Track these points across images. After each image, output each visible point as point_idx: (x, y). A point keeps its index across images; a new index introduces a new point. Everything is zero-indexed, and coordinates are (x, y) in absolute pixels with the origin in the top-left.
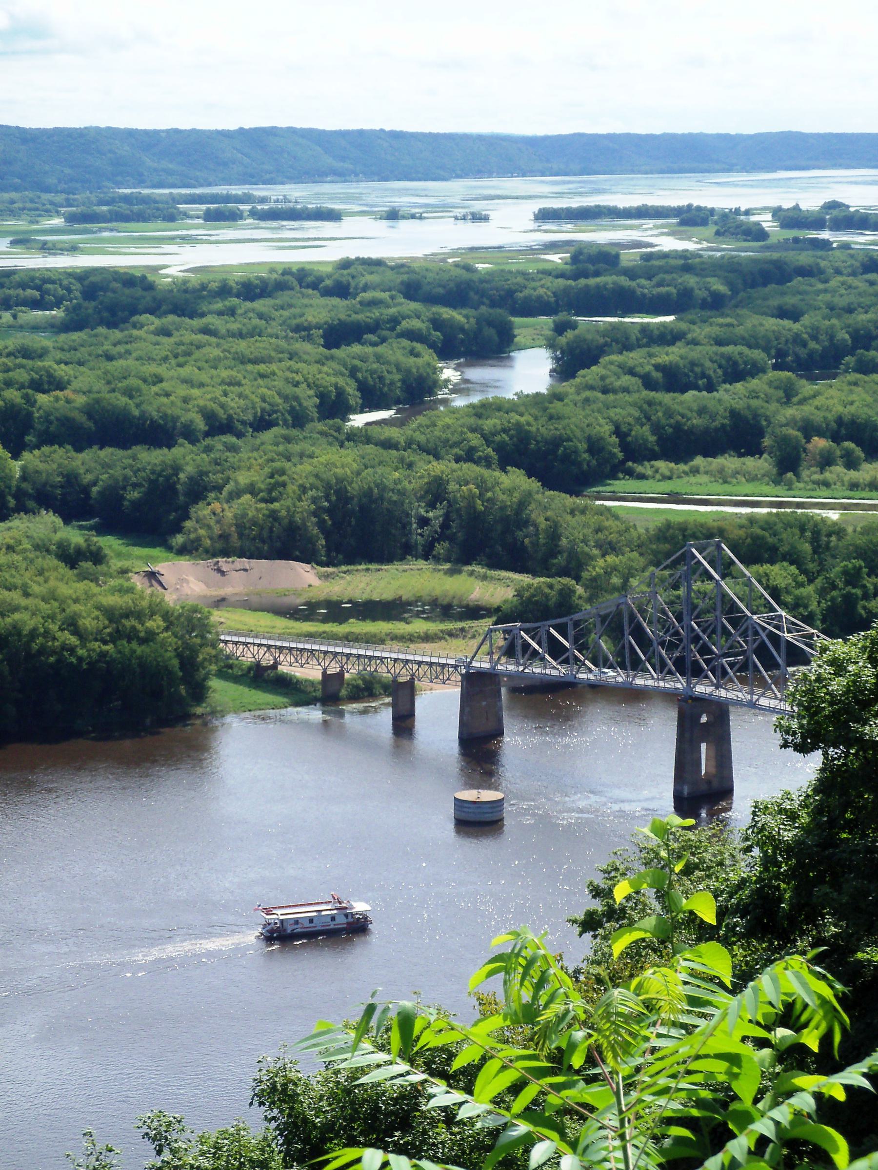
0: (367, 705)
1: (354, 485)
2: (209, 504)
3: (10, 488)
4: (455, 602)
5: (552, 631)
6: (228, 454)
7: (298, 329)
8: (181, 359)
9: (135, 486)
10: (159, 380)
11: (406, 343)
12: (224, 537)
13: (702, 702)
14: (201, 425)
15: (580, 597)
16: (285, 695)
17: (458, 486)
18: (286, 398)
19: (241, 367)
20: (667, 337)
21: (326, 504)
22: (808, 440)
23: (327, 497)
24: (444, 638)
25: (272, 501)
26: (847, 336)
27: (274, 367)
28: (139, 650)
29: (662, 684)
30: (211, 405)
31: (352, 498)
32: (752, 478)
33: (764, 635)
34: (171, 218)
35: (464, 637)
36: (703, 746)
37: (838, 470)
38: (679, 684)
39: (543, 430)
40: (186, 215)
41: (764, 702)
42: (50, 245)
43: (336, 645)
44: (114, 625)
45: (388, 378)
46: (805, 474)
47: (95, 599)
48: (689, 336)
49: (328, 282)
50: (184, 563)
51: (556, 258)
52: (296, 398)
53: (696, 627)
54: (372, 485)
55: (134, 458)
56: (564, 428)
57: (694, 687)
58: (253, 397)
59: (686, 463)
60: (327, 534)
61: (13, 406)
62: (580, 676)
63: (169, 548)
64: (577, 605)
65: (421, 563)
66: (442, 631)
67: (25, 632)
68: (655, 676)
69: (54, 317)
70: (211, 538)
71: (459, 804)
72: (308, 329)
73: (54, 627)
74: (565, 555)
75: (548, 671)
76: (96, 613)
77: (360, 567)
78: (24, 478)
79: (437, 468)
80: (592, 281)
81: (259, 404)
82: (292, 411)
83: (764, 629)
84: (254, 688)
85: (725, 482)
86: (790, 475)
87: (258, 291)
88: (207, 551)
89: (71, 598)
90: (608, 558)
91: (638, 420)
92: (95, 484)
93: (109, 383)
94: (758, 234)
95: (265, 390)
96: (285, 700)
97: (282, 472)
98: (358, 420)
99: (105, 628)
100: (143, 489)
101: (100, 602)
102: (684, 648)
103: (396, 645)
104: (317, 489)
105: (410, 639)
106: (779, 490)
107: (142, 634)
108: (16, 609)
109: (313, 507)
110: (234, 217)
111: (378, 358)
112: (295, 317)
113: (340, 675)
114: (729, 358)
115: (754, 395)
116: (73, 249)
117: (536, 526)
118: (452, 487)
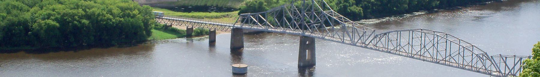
0: (200, 38)
5: (260, 15)
15: (265, 5)
16: (175, 34)
24: (222, 17)
28: (131, 20)
29: (295, 32)
36: (307, 50)
38: (300, 32)
41: (326, 38)
44: (123, 12)
47: (116, 4)
53: (306, 15)
57: (305, 33)
62: (269, 29)
67: (96, 14)
73: (105, 13)
75: (259, 28)
76: (117, 8)
83: (327, 15)
84: (165, 32)
99: (120, 13)
101: (118, 5)
102: (301, 21)
103: (207, 19)
105: (212, 18)
107: (132, 15)
108: (93, 7)
113: (192, 28)
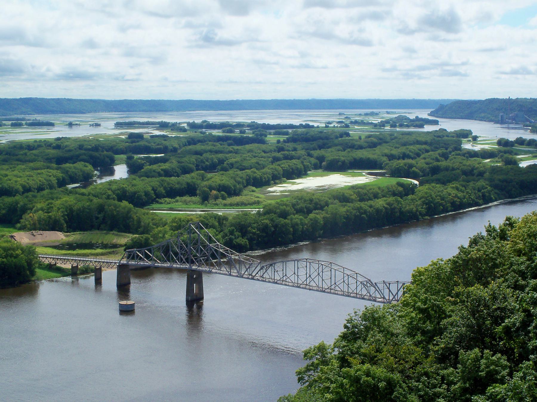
1: (75, 207)
2: (29, 214)
4: (109, 243)
6: (33, 198)
7: (47, 159)
9: (4, 209)
10: (7, 175)
11: (83, 163)
12: (34, 224)
13: (194, 271)
15: (151, 241)
16: (60, 273)
17: (108, 207)
18: (47, 180)
19: (33, 171)
20: (163, 160)
21: (66, 213)
22: (211, 191)
23: (66, 211)
25: (49, 213)
26: (217, 160)
27: (43, 171)
29: (182, 266)
31: (74, 211)
32: (195, 203)
33: (213, 250)
35: (114, 254)
36: (195, 285)
37: (220, 201)
38: (187, 266)
39: (130, 189)
40: (5, 125)
41: (213, 271)
43: (76, 257)
44: (6, 253)
46: (210, 201)
49: (54, 145)
50: (22, 233)
51: (123, 137)
52: (50, 181)
54: (81, 207)
56: (137, 189)
58: (37, 180)
59: (174, 199)
60: (66, 222)
63: (15, 228)
64: (150, 243)
65: (97, 231)
66: (107, 252)
68: (179, 264)
70: (30, 225)
71: (121, 305)
75: (145, 263)
77: (77, 233)
80: (137, 144)
81: (39, 183)
82: (49, 185)
83: (213, 248)
85: (186, 204)
86: (206, 202)
87: (32, 148)
88: (29, 229)
91: (159, 186)
95: (40, 178)
97: (52, 204)
100: (6, 210)
104: (63, 209)
106: (203, 206)
107: (15, 255)
109: (62, 214)
111: (75, 168)
113: (77, 266)
115: (193, 178)
117: (133, 219)
118: (106, 207)
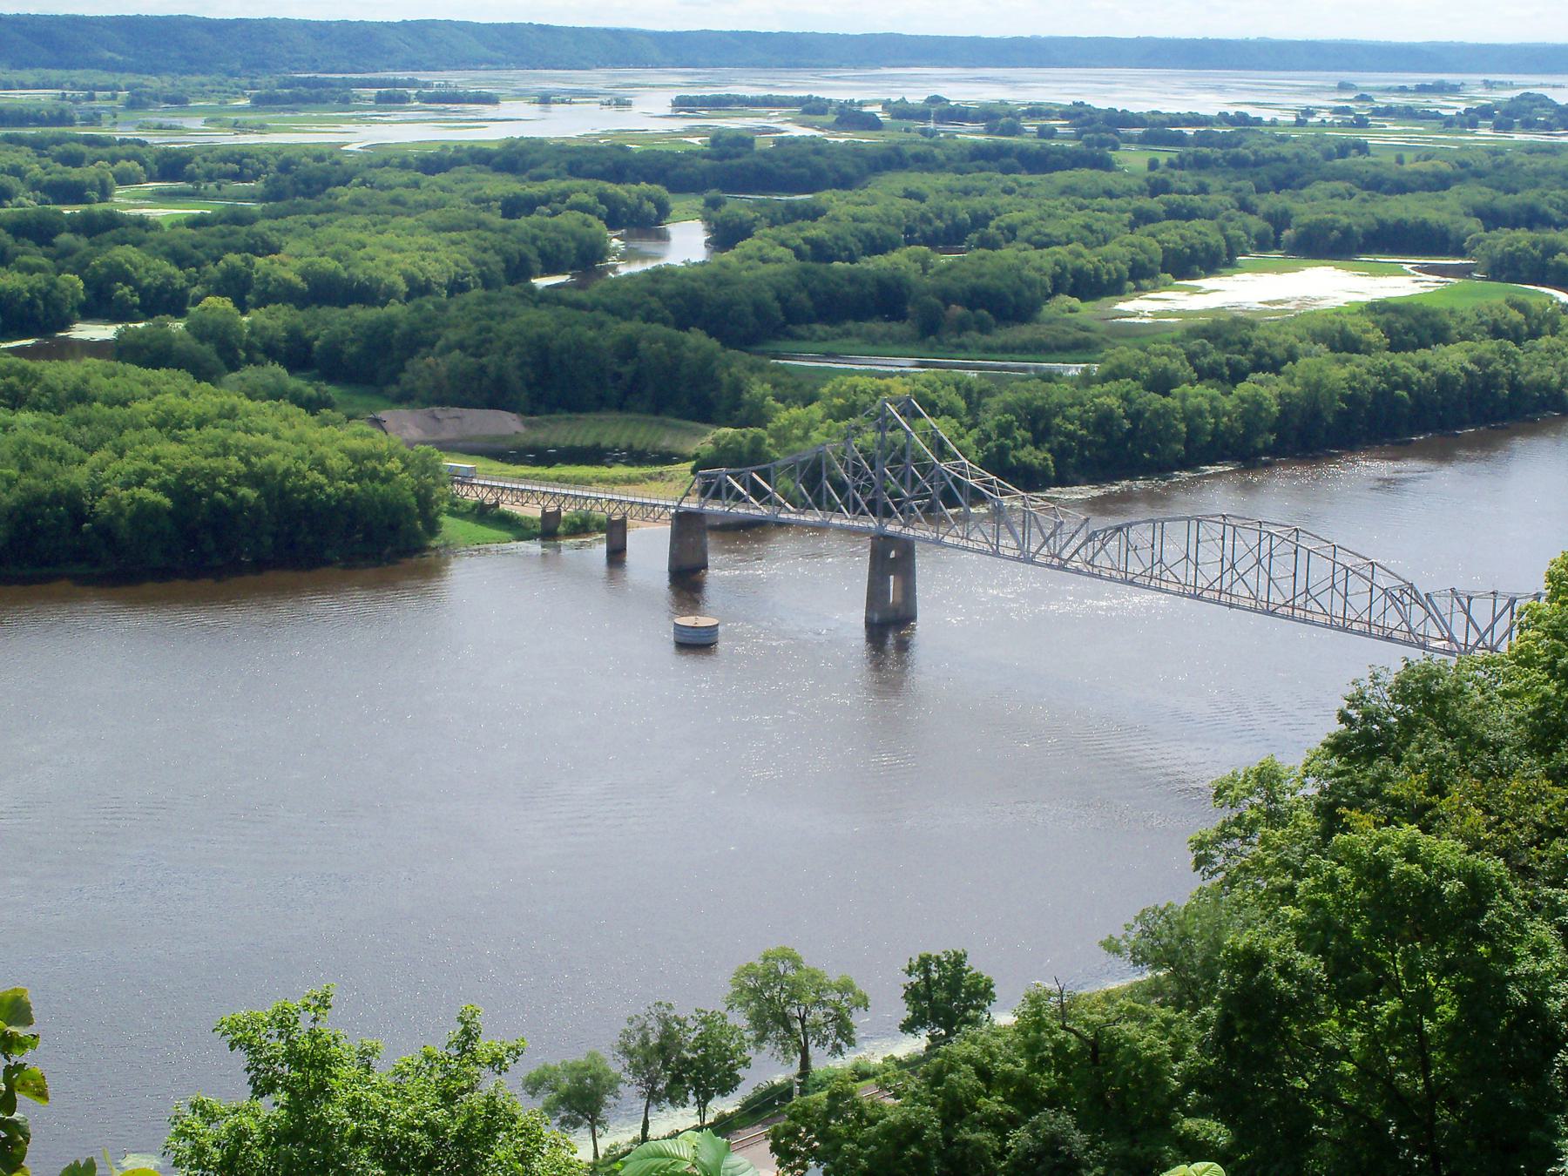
2: (424, 358)
3: (240, 341)
4: (649, 449)
5: (754, 475)
7: (477, 201)
8: (380, 227)
14: (403, 287)
15: (770, 445)
16: (509, 530)
22: (947, 306)
25: (481, 356)
26: (967, 216)
28: (381, 488)
29: (856, 524)
30: (415, 270)
34: (346, 100)
36: (892, 577)
38: (871, 523)
41: (948, 540)
42: (240, 123)
43: (554, 487)
44: (357, 467)
45: (565, 246)
48: (830, 213)
49: (497, 159)
55: (351, 315)
61: (234, 267)
62: (781, 516)
63: (387, 397)
65: (615, 415)
67: (279, 472)
69: (253, 188)
72: (486, 200)
73: (304, 467)
74: (747, 407)
75: (751, 512)
76: (341, 455)
78: (252, 333)
79: (627, 327)
81: (454, 268)
83: (949, 474)
89: (317, 441)
90: (791, 410)
92: (316, 338)
93: (317, 248)
94: (871, 123)
96: (509, 535)
97: (489, 330)
98: (541, 282)
103: (601, 487)
105: (615, 481)
107: (383, 474)
108: (269, 451)
110: (403, 99)
112: (474, 190)
113: (558, 513)
114: (868, 234)
116: (262, 128)
118: (643, 345)
